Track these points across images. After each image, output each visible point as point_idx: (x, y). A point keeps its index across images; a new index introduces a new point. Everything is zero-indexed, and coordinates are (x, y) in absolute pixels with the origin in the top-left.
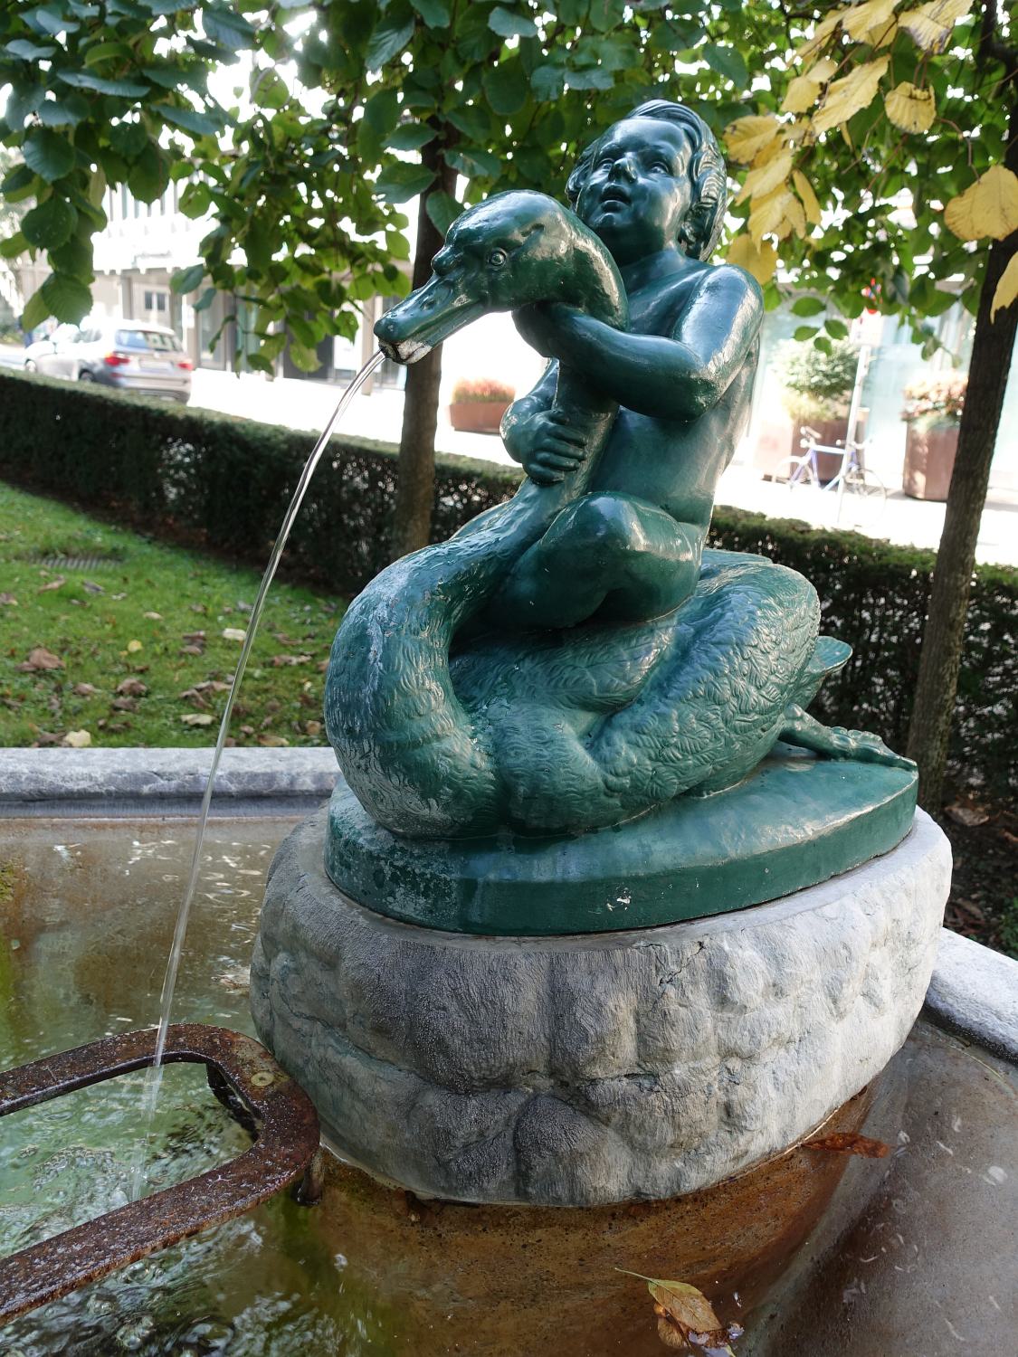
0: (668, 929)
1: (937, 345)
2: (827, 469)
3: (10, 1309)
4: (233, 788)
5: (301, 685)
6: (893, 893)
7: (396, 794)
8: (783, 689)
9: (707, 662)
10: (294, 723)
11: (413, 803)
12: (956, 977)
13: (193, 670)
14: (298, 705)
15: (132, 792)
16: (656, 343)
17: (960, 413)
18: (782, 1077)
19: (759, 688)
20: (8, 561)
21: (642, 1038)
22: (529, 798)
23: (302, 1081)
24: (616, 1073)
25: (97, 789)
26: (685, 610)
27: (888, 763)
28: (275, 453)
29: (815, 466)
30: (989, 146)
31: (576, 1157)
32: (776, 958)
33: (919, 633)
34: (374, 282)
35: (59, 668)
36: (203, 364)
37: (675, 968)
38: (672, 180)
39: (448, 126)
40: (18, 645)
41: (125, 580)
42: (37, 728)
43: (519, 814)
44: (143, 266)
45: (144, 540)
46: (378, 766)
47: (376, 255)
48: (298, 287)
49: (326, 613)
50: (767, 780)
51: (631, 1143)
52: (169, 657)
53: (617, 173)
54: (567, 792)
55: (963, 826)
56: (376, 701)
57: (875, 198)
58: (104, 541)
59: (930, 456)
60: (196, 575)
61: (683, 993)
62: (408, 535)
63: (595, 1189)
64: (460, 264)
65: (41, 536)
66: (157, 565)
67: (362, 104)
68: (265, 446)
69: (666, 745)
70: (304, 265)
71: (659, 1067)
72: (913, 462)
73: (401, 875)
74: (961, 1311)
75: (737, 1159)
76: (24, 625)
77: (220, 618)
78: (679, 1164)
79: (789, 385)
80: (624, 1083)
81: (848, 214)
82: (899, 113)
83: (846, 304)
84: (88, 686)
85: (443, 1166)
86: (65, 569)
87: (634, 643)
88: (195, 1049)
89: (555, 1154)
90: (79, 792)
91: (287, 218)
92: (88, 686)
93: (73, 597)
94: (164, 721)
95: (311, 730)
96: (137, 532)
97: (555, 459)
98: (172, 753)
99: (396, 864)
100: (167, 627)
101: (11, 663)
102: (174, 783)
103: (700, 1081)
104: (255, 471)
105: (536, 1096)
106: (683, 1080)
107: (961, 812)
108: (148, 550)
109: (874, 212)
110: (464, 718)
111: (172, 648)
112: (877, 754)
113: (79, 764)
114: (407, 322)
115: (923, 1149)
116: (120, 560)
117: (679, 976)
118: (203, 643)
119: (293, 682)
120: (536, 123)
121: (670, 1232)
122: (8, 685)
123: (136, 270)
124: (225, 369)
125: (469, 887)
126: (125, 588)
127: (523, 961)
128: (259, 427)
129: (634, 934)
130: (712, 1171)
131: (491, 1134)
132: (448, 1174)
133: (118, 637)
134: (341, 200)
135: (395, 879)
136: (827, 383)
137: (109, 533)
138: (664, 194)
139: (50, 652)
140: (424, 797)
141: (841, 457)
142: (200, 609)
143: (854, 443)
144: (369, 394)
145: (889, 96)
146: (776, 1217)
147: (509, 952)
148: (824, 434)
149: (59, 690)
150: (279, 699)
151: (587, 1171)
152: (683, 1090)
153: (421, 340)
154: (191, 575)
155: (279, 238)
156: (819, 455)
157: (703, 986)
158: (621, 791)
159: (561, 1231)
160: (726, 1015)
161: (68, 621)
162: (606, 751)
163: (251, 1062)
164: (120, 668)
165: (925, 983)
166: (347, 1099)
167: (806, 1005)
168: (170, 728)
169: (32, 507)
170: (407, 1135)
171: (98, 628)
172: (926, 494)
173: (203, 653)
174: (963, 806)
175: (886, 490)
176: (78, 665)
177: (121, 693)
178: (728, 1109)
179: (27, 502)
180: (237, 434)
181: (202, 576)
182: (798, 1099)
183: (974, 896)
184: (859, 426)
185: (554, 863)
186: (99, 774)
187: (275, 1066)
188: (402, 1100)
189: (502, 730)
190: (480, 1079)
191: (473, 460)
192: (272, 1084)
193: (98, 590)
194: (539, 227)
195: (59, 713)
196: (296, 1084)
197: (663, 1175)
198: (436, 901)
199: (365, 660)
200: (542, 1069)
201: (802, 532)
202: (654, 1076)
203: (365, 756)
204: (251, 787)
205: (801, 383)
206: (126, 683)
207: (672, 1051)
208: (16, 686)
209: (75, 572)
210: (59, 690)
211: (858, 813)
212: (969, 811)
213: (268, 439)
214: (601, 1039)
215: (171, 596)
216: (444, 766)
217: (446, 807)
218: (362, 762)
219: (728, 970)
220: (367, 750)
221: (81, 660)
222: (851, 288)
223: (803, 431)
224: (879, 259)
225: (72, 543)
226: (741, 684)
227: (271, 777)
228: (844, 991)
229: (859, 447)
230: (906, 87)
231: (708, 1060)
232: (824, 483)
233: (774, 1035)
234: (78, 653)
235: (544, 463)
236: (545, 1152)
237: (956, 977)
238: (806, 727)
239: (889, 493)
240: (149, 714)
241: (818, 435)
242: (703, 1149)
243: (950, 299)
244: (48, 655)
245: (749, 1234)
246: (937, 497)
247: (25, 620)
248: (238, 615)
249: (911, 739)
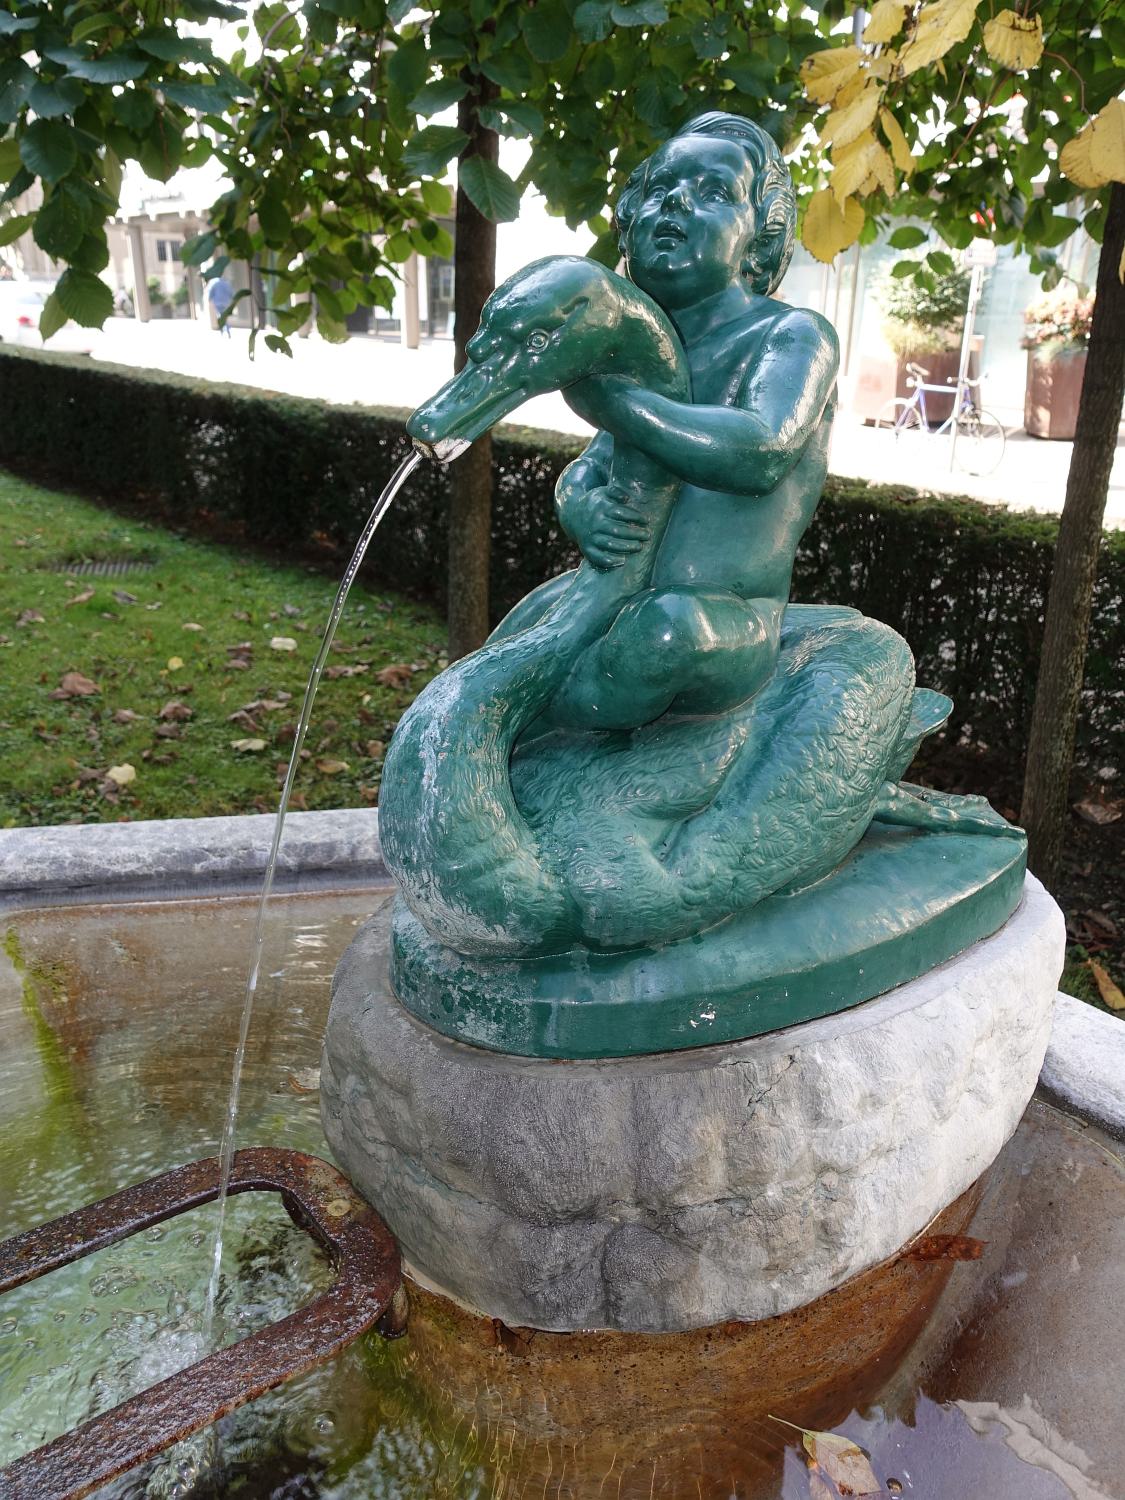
0: (756, 1041)
1: (1060, 274)
2: (937, 412)
3: (98, 1477)
5: (360, 699)
6: (999, 981)
7: (460, 923)
8: (872, 774)
9: (788, 755)
10: (354, 744)
11: (478, 929)
12: (1072, 1052)
13: (240, 688)
14: (357, 722)
16: (720, 416)
17: (1088, 336)
19: (846, 779)
20: (30, 571)
23: (378, 1206)
25: (145, 871)
26: (765, 695)
27: (994, 833)
28: (315, 433)
29: (923, 408)
30: (1112, 45)
32: (872, 1062)
33: (1042, 611)
34: (411, 240)
35: (96, 693)
37: (764, 1086)
38: (733, 209)
39: (482, 80)
40: (49, 669)
41: (160, 586)
42: (76, 764)
43: (591, 933)
44: (153, 211)
45: (177, 538)
46: (439, 896)
47: (413, 209)
48: (325, 250)
49: (382, 612)
50: (860, 867)
51: (724, 1267)
52: (213, 674)
53: (669, 206)
55: (1094, 825)
56: (433, 830)
57: (983, 108)
58: (132, 542)
59: (1054, 389)
60: (237, 576)
62: (467, 532)
63: (689, 1316)
65: (64, 539)
66: (194, 566)
67: (393, 38)
68: (304, 426)
69: (746, 851)
70: (334, 228)
71: (750, 1190)
72: (1036, 395)
73: (471, 1000)
74: (1074, 1425)
75: (836, 1276)
76: (54, 645)
77: (266, 626)
78: (775, 1285)
79: (891, 313)
80: (714, 1209)
81: (951, 127)
82: (1000, 45)
83: (952, 233)
84: (128, 713)
85: (530, 1298)
86: (93, 578)
87: (708, 741)
88: (267, 1177)
91: (309, 173)
92: (128, 713)
93: (104, 609)
94: (213, 749)
95: (374, 750)
96: (169, 528)
98: (224, 822)
99: (465, 988)
100: (210, 640)
101: (42, 691)
103: (795, 1201)
104: (294, 454)
106: (776, 1202)
107: (1091, 809)
108: (182, 548)
109: (984, 123)
110: (528, 835)
111: (216, 663)
112: (981, 825)
113: (124, 844)
115: (1037, 1243)
116: (153, 563)
117: (768, 1094)
118: (249, 656)
119: (350, 696)
120: (582, 68)
121: (770, 1350)
122: (42, 716)
123: (146, 217)
125: (542, 1013)
126: (160, 595)
127: (603, 1088)
128: (297, 403)
129: (720, 1050)
130: (811, 1291)
131: (578, 1265)
132: (535, 1305)
133: (156, 654)
134: (369, 148)
135: (464, 1004)
136: (936, 309)
137: (138, 530)
138: (723, 225)
139: (84, 676)
140: (489, 923)
141: (953, 395)
142: (243, 616)
143: (967, 380)
144: (416, 348)
145: (988, 26)
146: (881, 1327)
147: (588, 1078)
148: (932, 372)
149: (96, 718)
150: (336, 716)
151: (680, 1298)
152: (775, 1214)
153: (459, 437)
154: (231, 576)
155: (301, 196)
156: (928, 395)
157: (795, 1103)
158: (702, 902)
159: (655, 1355)
160: (822, 1130)
161: (101, 638)
163: (326, 1189)
164: (160, 690)
165: (1036, 1064)
166: (427, 1229)
168: (220, 757)
169: (51, 505)
170: (491, 1269)
171: (133, 645)
172: (1050, 432)
173: (250, 667)
174: (1093, 802)
175: (1004, 430)
176: (115, 689)
177: (165, 719)
178: (824, 1226)
179: (45, 500)
180: (272, 413)
181: (243, 576)
182: (901, 1209)
183: (1105, 906)
184: (972, 356)
185: (632, 981)
186: (146, 855)
187: (351, 1192)
188: (483, 1233)
190: (564, 1212)
191: (536, 431)
192: (348, 1214)
193: (131, 600)
194: (584, 300)
195: (100, 746)
196: (374, 1210)
198: (508, 1025)
199: (417, 788)
201: (908, 503)
202: (746, 1199)
205: (906, 310)
206: (169, 706)
207: (764, 1173)
208: (51, 716)
209: (104, 580)
210: (96, 718)
211: (954, 900)
212: (1100, 808)
213: (305, 417)
215: (211, 602)
217: (514, 932)
218: (422, 892)
219: (822, 1085)
220: (426, 880)
221: (118, 683)
222: (958, 214)
223: (909, 368)
224: (991, 179)
225: (99, 546)
226: (827, 776)
227: (330, 848)
228: (948, 1094)
229: (973, 383)
230: (1007, 16)
231: (802, 1178)
232: (934, 425)
233: (873, 1147)
234: (115, 676)
237: (1072, 1052)
238: (901, 805)
239: (1008, 434)
240: (197, 742)
241: (925, 372)
243: (1070, 225)
244: (82, 679)
245: (852, 1347)
246: (1064, 435)
247: (54, 640)
248: (285, 620)
249: (1032, 739)
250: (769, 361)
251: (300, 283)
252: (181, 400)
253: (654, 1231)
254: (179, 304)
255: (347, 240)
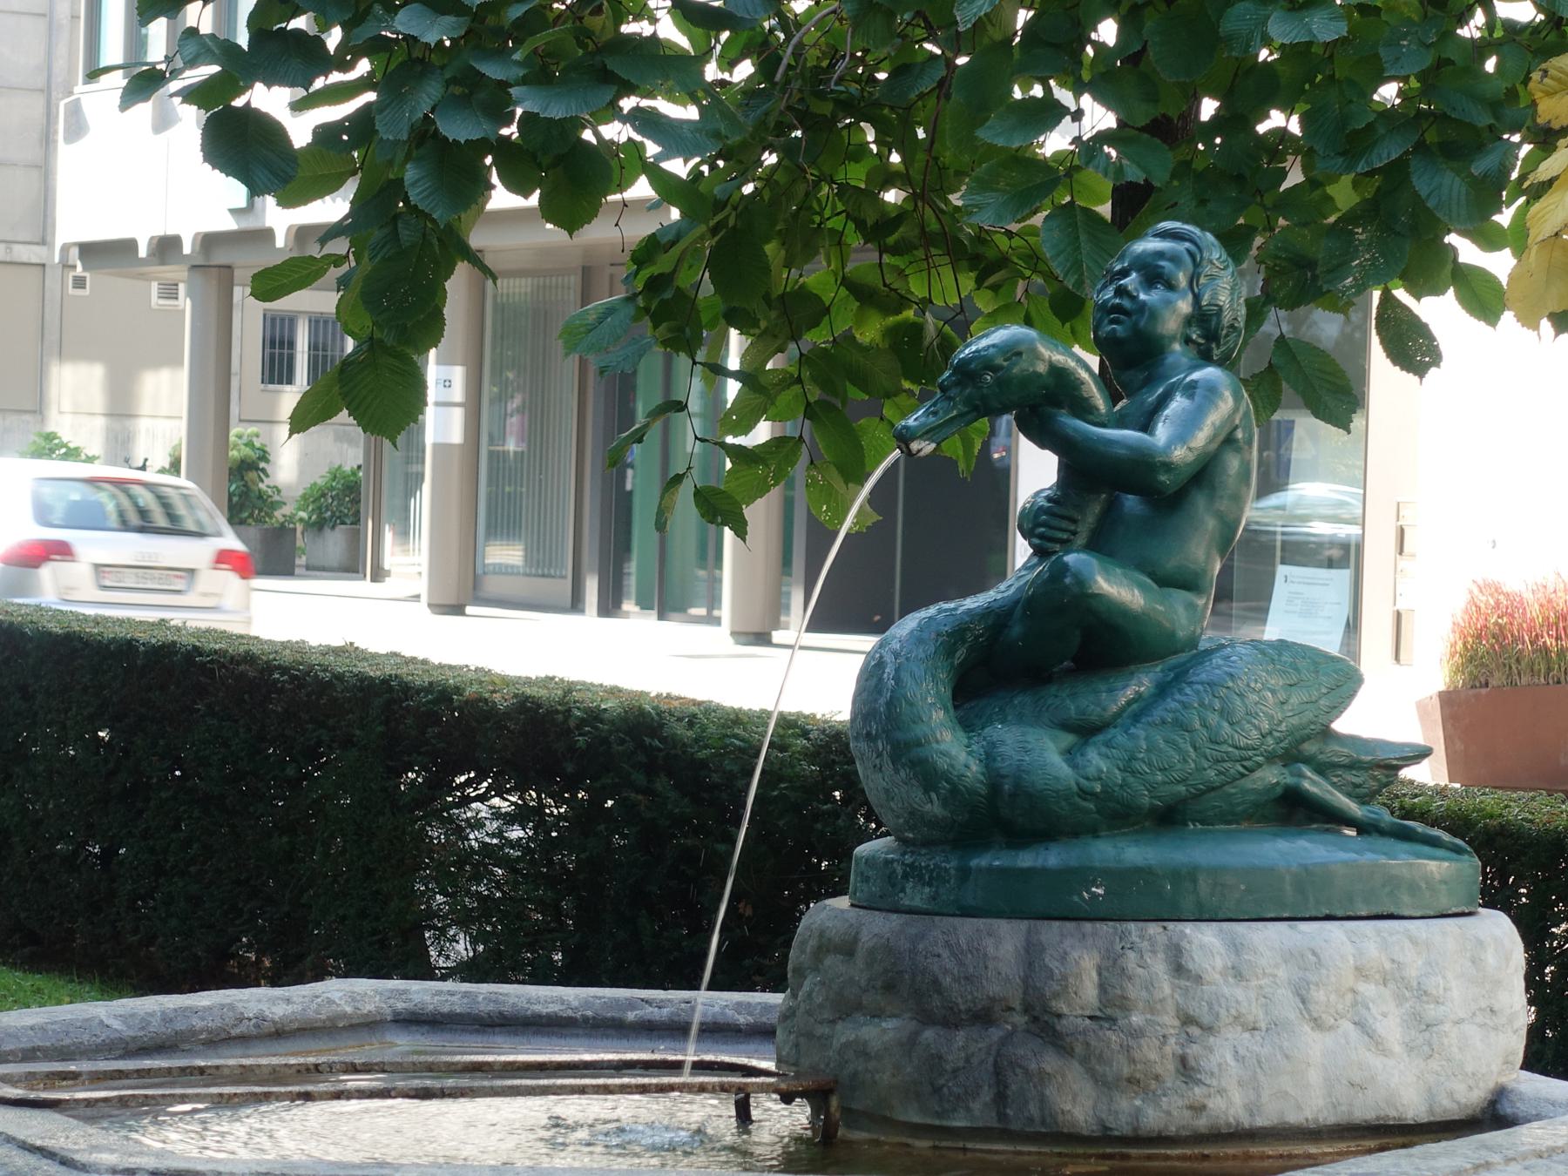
4: (742, 1020)
15: (613, 1019)
18: (1242, 1051)
21: (1103, 987)
22: (1013, 795)
24: (1080, 1012)
25: (570, 1013)
31: (1043, 1077)
36: (492, 585)
46: (889, 762)
48: (849, 337)
53: (1121, 292)
54: (1045, 790)
61: (1142, 957)
64: (957, 384)
69: (1133, 758)
71: (1117, 1013)
78: (1138, 1102)
85: (937, 1090)
89: (1026, 1072)
90: (548, 1016)
97: (1051, 533)
102: (665, 1011)
103: (1156, 1030)
105: (1014, 1031)
106: (1139, 1026)
114: (917, 427)
124: (575, 604)
131: (975, 1061)
140: (926, 791)
152: (1137, 1034)
157: (1161, 955)
160: (1183, 983)
162: (1079, 759)
167: (1270, 996)
178: (1183, 1060)
189: (993, 743)
190: (969, 1010)
197: (1127, 1110)
200: (1018, 1008)
202: (1112, 1020)
203: (879, 755)
204: (764, 1019)
214: (1065, 978)
216: (942, 763)
218: (878, 762)
235: (1041, 537)
236: (1018, 1071)
242: (1159, 1092)
250: (1178, 404)
251: (786, 397)
252: (431, 717)
253: (1038, 1036)
254: (318, 526)
255: (892, 320)
